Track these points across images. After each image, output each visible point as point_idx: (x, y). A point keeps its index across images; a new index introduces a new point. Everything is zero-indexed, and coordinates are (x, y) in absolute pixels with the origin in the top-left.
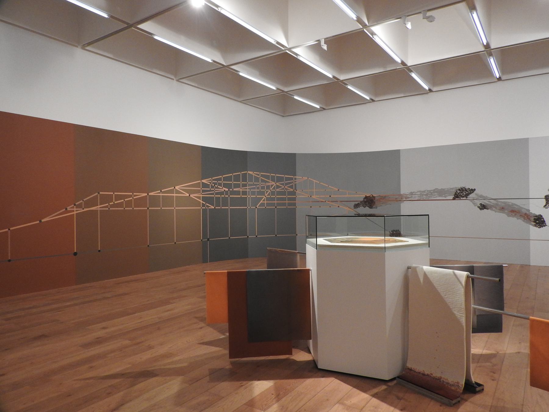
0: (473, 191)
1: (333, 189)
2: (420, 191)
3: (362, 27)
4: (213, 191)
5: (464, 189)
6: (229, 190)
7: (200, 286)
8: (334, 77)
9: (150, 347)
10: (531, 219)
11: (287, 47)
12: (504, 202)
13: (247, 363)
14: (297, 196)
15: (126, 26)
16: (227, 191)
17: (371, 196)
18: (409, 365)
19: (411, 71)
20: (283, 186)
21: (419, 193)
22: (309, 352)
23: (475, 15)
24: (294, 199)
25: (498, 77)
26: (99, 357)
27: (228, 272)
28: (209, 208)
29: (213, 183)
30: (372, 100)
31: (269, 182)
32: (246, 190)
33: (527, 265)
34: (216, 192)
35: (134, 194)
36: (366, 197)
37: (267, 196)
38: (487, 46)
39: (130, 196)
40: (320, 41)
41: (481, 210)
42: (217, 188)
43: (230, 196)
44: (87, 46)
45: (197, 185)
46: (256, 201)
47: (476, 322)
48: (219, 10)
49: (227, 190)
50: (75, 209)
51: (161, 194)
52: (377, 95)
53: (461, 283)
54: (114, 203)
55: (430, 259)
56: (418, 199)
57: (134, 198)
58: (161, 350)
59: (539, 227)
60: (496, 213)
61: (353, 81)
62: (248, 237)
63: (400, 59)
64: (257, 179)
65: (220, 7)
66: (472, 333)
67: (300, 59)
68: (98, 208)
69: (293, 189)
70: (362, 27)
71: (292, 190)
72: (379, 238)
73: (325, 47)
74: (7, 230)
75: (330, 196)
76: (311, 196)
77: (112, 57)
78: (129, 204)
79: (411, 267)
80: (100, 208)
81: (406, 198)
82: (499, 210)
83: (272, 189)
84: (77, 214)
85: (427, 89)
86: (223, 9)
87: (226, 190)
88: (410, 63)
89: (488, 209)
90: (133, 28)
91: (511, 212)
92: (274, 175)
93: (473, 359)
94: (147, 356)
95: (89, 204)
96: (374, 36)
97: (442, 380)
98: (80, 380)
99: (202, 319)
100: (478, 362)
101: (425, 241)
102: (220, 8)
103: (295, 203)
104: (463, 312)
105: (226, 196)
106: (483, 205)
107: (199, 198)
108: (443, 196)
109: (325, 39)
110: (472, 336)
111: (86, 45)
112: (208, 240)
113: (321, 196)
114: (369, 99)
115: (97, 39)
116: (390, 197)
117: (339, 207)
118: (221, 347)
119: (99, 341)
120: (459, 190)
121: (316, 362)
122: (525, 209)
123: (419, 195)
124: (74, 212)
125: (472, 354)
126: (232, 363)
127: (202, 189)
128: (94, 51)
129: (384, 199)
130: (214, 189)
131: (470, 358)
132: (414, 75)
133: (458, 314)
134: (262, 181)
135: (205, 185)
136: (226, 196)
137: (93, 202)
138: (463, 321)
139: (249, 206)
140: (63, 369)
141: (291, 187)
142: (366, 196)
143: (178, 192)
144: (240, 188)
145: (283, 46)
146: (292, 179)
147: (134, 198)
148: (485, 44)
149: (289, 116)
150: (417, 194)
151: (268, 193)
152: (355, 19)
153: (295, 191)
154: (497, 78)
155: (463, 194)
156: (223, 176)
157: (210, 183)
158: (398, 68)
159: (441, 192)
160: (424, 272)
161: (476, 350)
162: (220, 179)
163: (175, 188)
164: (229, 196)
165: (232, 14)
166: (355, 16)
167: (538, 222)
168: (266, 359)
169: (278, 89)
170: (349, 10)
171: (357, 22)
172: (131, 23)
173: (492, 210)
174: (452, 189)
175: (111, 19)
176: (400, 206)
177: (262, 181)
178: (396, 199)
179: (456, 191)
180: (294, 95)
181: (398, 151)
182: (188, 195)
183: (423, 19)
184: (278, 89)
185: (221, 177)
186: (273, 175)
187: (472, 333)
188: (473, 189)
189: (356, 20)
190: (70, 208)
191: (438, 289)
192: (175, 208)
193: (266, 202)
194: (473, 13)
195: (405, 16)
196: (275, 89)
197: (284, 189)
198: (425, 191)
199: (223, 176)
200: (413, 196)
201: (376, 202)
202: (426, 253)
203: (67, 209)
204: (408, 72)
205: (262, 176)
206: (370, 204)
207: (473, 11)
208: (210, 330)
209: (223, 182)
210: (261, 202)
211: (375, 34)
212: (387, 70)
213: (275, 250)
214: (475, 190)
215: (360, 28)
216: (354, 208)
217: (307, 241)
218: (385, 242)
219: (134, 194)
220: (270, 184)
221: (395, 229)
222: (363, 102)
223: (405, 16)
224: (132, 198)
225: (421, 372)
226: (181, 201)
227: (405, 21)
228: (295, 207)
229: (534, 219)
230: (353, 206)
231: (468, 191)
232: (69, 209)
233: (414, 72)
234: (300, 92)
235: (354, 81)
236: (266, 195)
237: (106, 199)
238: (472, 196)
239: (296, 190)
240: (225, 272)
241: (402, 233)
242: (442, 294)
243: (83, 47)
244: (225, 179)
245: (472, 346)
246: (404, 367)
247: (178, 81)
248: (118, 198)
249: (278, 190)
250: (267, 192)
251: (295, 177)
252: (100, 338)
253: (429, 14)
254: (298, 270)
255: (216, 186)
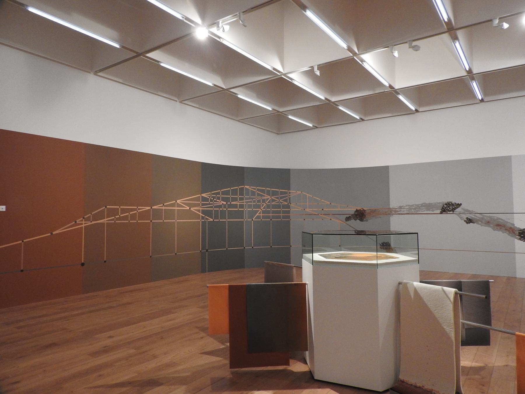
0: (459, 205)
1: (326, 203)
2: (409, 205)
3: (352, 55)
4: (212, 204)
5: (451, 204)
6: (227, 203)
7: (199, 296)
8: (326, 99)
9: (155, 357)
10: (516, 232)
11: (282, 73)
12: (490, 216)
13: (246, 373)
14: (291, 210)
15: (136, 54)
16: (226, 205)
17: (362, 209)
18: (401, 377)
19: (399, 94)
20: (280, 201)
21: (407, 207)
22: (306, 363)
23: (457, 44)
24: (289, 212)
25: (480, 99)
26: (107, 365)
27: (229, 285)
28: (208, 220)
29: (212, 197)
30: (362, 119)
31: (265, 196)
32: (243, 203)
33: (512, 277)
34: (214, 205)
35: (139, 207)
36: (357, 211)
37: (262, 209)
38: (470, 72)
39: (135, 210)
40: (314, 67)
41: (467, 224)
42: (216, 201)
43: (228, 209)
44: (99, 72)
45: (197, 199)
46: (252, 214)
47: (465, 335)
48: (221, 41)
49: (225, 203)
50: (84, 222)
51: (163, 208)
52: (366, 114)
53: (449, 299)
54: (120, 216)
55: (420, 270)
56: (407, 213)
57: (139, 211)
58: (166, 360)
59: (524, 240)
60: (482, 227)
61: (343, 102)
62: (244, 248)
63: (388, 83)
64: (253, 193)
65: (222, 38)
66: (462, 345)
67: (294, 83)
68: (105, 221)
69: (287, 202)
70: (352, 55)
71: (286, 203)
72: (371, 254)
73: (318, 73)
74: (21, 242)
75: (323, 209)
76: (304, 210)
77: (122, 82)
78: (133, 217)
79: (402, 282)
80: (107, 221)
81: (395, 212)
82: (485, 224)
83: (267, 203)
84: (85, 226)
85: (414, 110)
86: (225, 40)
87: (224, 204)
88: (397, 86)
89: (474, 223)
90: (141, 57)
91: (496, 226)
92: (270, 189)
93: (463, 372)
94: (152, 365)
95: (96, 217)
96: (363, 63)
97: (433, 392)
98: (91, 388)
99: (204, 329)
100: (467, 375)
101: (415, 258)
102: (221, 39)
103: (289, 216)
104: (452, 327)
105: (224, 209)
106: (469, 219)
107: (199, 211)
108: (431, 210)
109: (318, 65)
110: (461, 349)
111: (98, 71)
112: (207, 251)
113: (314, 209)
114: (359, 118)
115: (107, 67)
116: (380, 211)
117: (331, 219)
118: (221, 357)
119: (106, 350)
120: (446, 204)
121: (313, 374)
122: (509, 223)
123: (408, 209)
124: (83, 224)
125: (461, 366)
126: (232, 373)
127: (202, 202)
128: (105, 76)
129: (374, 212)
130: (212, 203)
131: (460, 372)
132: (401, 97)
133: (447, 328)
134: (258, 195)
135: (204, 199)
136: (224, 209)
137: (100, 216)
138: (452, 335)
139: (246, 219)
140: (74, 377)
141: (286, 200)
142: (357, 209)
143: (179, 205)
144: (237, 202)
145: (279, 71)
146: (286, 193)
147: (139, 211)
148: (468, 69)
149: (283, 133)
150: (405, 208)
151: (264, 206)
152: (346, 48)
153: (289, 204)
154: (479, 99)
155: (450, 208)
156: (222, 190)
157: (210, 197)
158: (386, 91)
159: (429, 207)
160: (414, 289)
161: (465, 362)
162: (218, 193)
163: (176, 201)
164: (227, 209)
165: (231, 43)
166: (346, 45)
167: (522, 235)
168: (264, 369)
169: (273, 109)
170: (343, 42)
171: (348, 51)
172: (140, 52)
173: (478, 224)
174: (439, 203)
175: (122, 48)
176: (389, 219)
177: (258, 195)
178: (386, 212)
179: (443, 206)
180: (288, 115)
181: (387, 167)
182: (188, 208)
183: (409, 48)
184: (273, 109)
185: (220, 192)
186: (269, 189)
187: (462, 345)
188: (459, 203)
189: (347, 49)
190: (79, 221)
191: (428, 305)
192: (176, 221)
193: (261, 215)
194: (456, 43)
195: (392, 45)
196: (271, 110)
197: (279, 203)
198: (413, 205)
199: (222, 190)
200: (402, 210)
201: (366, 215)
202: (416, 268)
203: (76, 222)
204: (396, 94)
205: (258, 190)
206: (361, 218)
207: (456, 41)
208: (211, 340)
209: (222, 196)
210: (257, 214)
211: (365, 61)
212: (375, 93)
213: (272, 263)
214: (461, 204)
215: (350, 56)
216: (346, 221)
217: (303, 256)
218: (377, 258)
219: (139, 207)
220: (266, 198)
221: (385, 241)
222: (353, 121)
223: (392, 45)
224: (136, 212)
225: (414, 384)
226: (183, 214)
227: (392, 50)
228: (290, 220)
229: (519, 233)
230: (345, 219)
231: (455, 206)
232: (78, 222)
233: (401, 95)
234: (295, 113)
235: (345, 103)
236: (262, 208)
237: (113, 212)
238: (458, 210)
239: (290, 204)
240: (227, 285)
241: (392, 245)
242: (432, 310)
243: (96, 73)
244: (223, 193)
245: (461, 358)
246: (397, 380)
247: (181, 102)
248: (124, 211)
249: (273, 203)
250: (263, 205)
251: (289, 191)
252: (107, 346)
253: (414, 43)
254: (295, 284)
255: (215, 199)
